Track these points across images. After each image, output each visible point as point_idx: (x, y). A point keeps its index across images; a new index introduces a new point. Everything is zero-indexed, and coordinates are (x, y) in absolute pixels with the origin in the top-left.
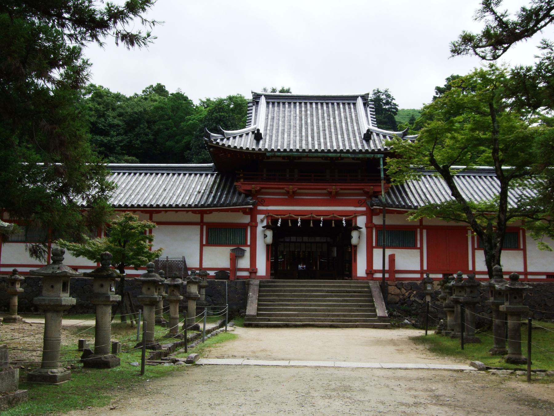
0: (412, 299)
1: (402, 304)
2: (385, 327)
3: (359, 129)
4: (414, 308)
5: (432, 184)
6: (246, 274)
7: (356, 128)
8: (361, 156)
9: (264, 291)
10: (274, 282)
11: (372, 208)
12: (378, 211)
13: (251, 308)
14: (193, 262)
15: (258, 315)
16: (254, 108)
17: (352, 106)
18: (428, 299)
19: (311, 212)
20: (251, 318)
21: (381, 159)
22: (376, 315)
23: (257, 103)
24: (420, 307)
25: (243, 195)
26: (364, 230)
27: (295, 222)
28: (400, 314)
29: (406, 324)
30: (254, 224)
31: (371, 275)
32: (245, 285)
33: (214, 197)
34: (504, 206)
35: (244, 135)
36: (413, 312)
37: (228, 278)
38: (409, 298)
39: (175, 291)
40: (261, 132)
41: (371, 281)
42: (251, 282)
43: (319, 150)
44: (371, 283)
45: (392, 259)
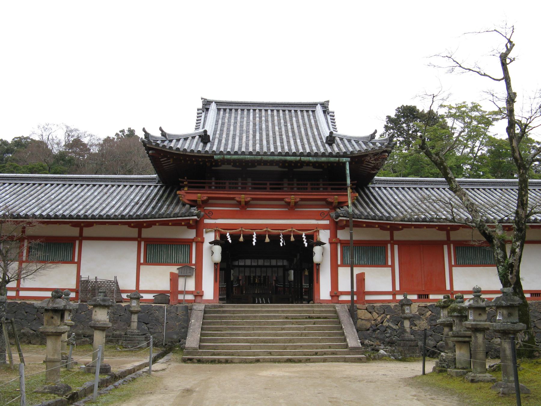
0: (386, 324)
1: (374, 331)
2: (360, 360)
3: (319, 134)
4: (388, 335)
5: (401, 196)
6: (190, 297)
7: (316, 133)
8: (324, 159)
9: (210, 318)
10: (222, 307)
11: (337, 220)
12: (345, 222)
13: (192, 339)
14: (127, 283)
15: (200, 347)
16: (203, 114)
17: (311, 113)
18: (407, 324)
19: (267, 226)
20: (193, 351)
21: (348, 163)
22: (347, 345)
23: (207, 109)
24: (395, 333)
25: (188, 206)
26: (327, 246)
27: (248, 238)
28: (372, 343)
29: (383, 355)
30: (199, 239)
31: (336, 298)
32: (188, 310)
33: (154, 208)
34: (525, 198)
35: (190, 138)
36: (387, 339)
37: (167, 302)
38: (382, 323)
39: (55, 317)
40: (208, 134)
41: (338, 305)
42: (195, 307)
43: (276, 153)
44: (338, 307)
45: (361, 279)
